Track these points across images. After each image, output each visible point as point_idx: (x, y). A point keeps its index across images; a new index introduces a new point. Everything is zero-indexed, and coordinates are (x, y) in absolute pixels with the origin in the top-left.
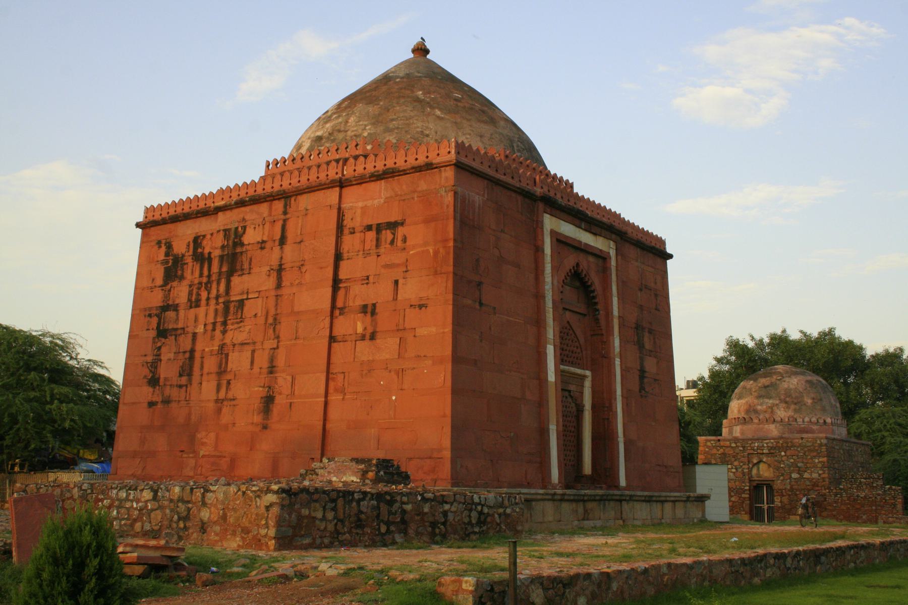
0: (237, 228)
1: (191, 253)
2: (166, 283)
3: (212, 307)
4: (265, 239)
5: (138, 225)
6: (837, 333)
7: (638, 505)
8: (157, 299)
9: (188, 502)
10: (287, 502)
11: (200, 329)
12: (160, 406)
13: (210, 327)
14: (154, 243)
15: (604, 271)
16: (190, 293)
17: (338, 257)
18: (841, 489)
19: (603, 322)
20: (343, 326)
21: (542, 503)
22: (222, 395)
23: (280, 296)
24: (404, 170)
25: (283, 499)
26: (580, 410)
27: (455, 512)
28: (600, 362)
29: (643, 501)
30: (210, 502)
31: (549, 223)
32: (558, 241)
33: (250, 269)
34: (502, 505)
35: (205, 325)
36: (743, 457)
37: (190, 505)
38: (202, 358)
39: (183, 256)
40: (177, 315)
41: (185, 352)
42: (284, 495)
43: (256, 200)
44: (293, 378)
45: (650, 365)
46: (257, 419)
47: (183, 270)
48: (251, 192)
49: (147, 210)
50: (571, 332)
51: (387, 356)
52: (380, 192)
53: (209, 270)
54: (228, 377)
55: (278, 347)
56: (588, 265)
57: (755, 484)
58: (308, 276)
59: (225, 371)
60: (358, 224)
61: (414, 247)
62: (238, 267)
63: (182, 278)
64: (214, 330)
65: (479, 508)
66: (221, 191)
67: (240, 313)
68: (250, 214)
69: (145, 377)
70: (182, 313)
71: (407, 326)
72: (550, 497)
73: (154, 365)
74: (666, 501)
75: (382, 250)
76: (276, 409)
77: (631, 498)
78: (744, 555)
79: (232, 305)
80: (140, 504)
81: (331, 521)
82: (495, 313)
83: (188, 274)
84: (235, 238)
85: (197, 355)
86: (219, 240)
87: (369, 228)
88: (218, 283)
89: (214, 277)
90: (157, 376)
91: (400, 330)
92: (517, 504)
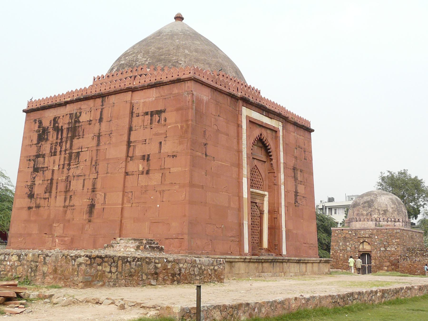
0: (76, 113)
1: (52, 126)
2: (38, 143)
3: (63, 156)
4: (91, 119)
5: (24, 111)
6: (408, 173)
7: (292, 265)
8: (33, 151)
9: (37, 262)
10: (89, 262)
11: (56, 168)
12: (34, 209)
13: (61, 167)
14: (32, 121)
15: (277, 138)
16: (51, 148)
17: (130, 129)
18: (407, 256)
19: (275, 166)
20: (132, 167)
21: (239, 264)
22: (67, 203)
23: (99, 150)
24: (165, 82)
25: (87, 261)
26: (262, 213)
27: (186, 268)
28: (273, 188)
29: (296, 262)
30: (48, 262)
31: (246, 112)
32: (250, 121)
33: (83, 135)
34: (212, 264)
35: (59, 165)
36: (355, 238)
37: (37, 264)
38: (57, 183)
39: (48, 128)
40: (44, 160)
41: (48, 180)
42: (87, 259)
43: (86, 99)
44: (105, 194)
45: (301, 189)
46: (86, 217)
47: (47, 135)
48: (84, 94)
49: (29, 103)
50: (257, 171)
51: (155, 183)
52: (153, 93)
53: (62, 136)
54: (71, 194)
55: (97, 178)
56: (267, 135)
57: (361, 253)
58: (114, 140)
59: (69, 191)
60: (141, 111)
61: (170, 124)
62: (77, 134)
63: (47, 140)
64: (63, 168)
65: (199, 266)
66: (68, 93)
67: (77, 159)
68: (84, 105)
69: (27, 193)
70: (46, 159)
71: (166, 167)
72: (243, 260)
73: (31, 187)
74: (308, 263)
75: (153, 126)
76: (95, 211)
77: (289, 261)
78: (130, 318)
79: (73, 155)
80: (11, 263)
81: (114, 273)
82: (214, 161)
83: (50, 138)
84: (75, 119)
85: (54, 182)
86: (67, 119)
87: (147, 114)
88: (66, 143)
89: (64, 140)
90: (33, 193)
91: (162, 169)
92: (220, 264)
